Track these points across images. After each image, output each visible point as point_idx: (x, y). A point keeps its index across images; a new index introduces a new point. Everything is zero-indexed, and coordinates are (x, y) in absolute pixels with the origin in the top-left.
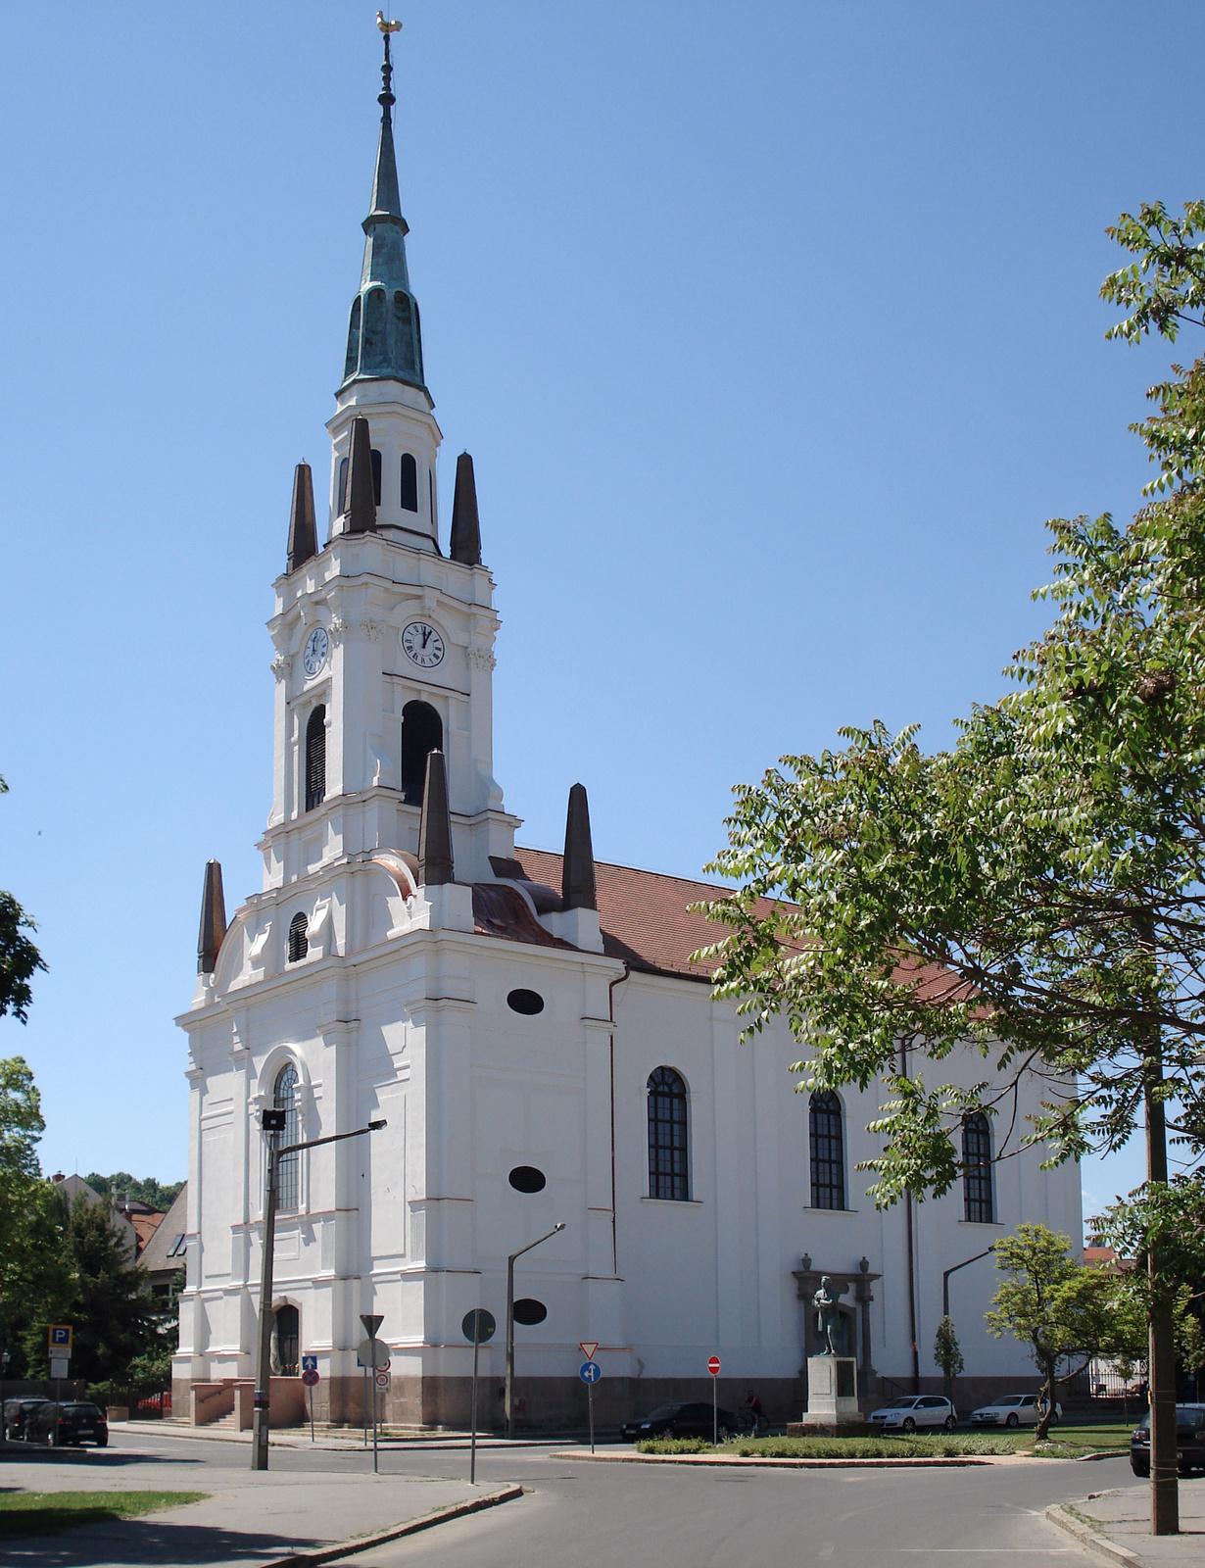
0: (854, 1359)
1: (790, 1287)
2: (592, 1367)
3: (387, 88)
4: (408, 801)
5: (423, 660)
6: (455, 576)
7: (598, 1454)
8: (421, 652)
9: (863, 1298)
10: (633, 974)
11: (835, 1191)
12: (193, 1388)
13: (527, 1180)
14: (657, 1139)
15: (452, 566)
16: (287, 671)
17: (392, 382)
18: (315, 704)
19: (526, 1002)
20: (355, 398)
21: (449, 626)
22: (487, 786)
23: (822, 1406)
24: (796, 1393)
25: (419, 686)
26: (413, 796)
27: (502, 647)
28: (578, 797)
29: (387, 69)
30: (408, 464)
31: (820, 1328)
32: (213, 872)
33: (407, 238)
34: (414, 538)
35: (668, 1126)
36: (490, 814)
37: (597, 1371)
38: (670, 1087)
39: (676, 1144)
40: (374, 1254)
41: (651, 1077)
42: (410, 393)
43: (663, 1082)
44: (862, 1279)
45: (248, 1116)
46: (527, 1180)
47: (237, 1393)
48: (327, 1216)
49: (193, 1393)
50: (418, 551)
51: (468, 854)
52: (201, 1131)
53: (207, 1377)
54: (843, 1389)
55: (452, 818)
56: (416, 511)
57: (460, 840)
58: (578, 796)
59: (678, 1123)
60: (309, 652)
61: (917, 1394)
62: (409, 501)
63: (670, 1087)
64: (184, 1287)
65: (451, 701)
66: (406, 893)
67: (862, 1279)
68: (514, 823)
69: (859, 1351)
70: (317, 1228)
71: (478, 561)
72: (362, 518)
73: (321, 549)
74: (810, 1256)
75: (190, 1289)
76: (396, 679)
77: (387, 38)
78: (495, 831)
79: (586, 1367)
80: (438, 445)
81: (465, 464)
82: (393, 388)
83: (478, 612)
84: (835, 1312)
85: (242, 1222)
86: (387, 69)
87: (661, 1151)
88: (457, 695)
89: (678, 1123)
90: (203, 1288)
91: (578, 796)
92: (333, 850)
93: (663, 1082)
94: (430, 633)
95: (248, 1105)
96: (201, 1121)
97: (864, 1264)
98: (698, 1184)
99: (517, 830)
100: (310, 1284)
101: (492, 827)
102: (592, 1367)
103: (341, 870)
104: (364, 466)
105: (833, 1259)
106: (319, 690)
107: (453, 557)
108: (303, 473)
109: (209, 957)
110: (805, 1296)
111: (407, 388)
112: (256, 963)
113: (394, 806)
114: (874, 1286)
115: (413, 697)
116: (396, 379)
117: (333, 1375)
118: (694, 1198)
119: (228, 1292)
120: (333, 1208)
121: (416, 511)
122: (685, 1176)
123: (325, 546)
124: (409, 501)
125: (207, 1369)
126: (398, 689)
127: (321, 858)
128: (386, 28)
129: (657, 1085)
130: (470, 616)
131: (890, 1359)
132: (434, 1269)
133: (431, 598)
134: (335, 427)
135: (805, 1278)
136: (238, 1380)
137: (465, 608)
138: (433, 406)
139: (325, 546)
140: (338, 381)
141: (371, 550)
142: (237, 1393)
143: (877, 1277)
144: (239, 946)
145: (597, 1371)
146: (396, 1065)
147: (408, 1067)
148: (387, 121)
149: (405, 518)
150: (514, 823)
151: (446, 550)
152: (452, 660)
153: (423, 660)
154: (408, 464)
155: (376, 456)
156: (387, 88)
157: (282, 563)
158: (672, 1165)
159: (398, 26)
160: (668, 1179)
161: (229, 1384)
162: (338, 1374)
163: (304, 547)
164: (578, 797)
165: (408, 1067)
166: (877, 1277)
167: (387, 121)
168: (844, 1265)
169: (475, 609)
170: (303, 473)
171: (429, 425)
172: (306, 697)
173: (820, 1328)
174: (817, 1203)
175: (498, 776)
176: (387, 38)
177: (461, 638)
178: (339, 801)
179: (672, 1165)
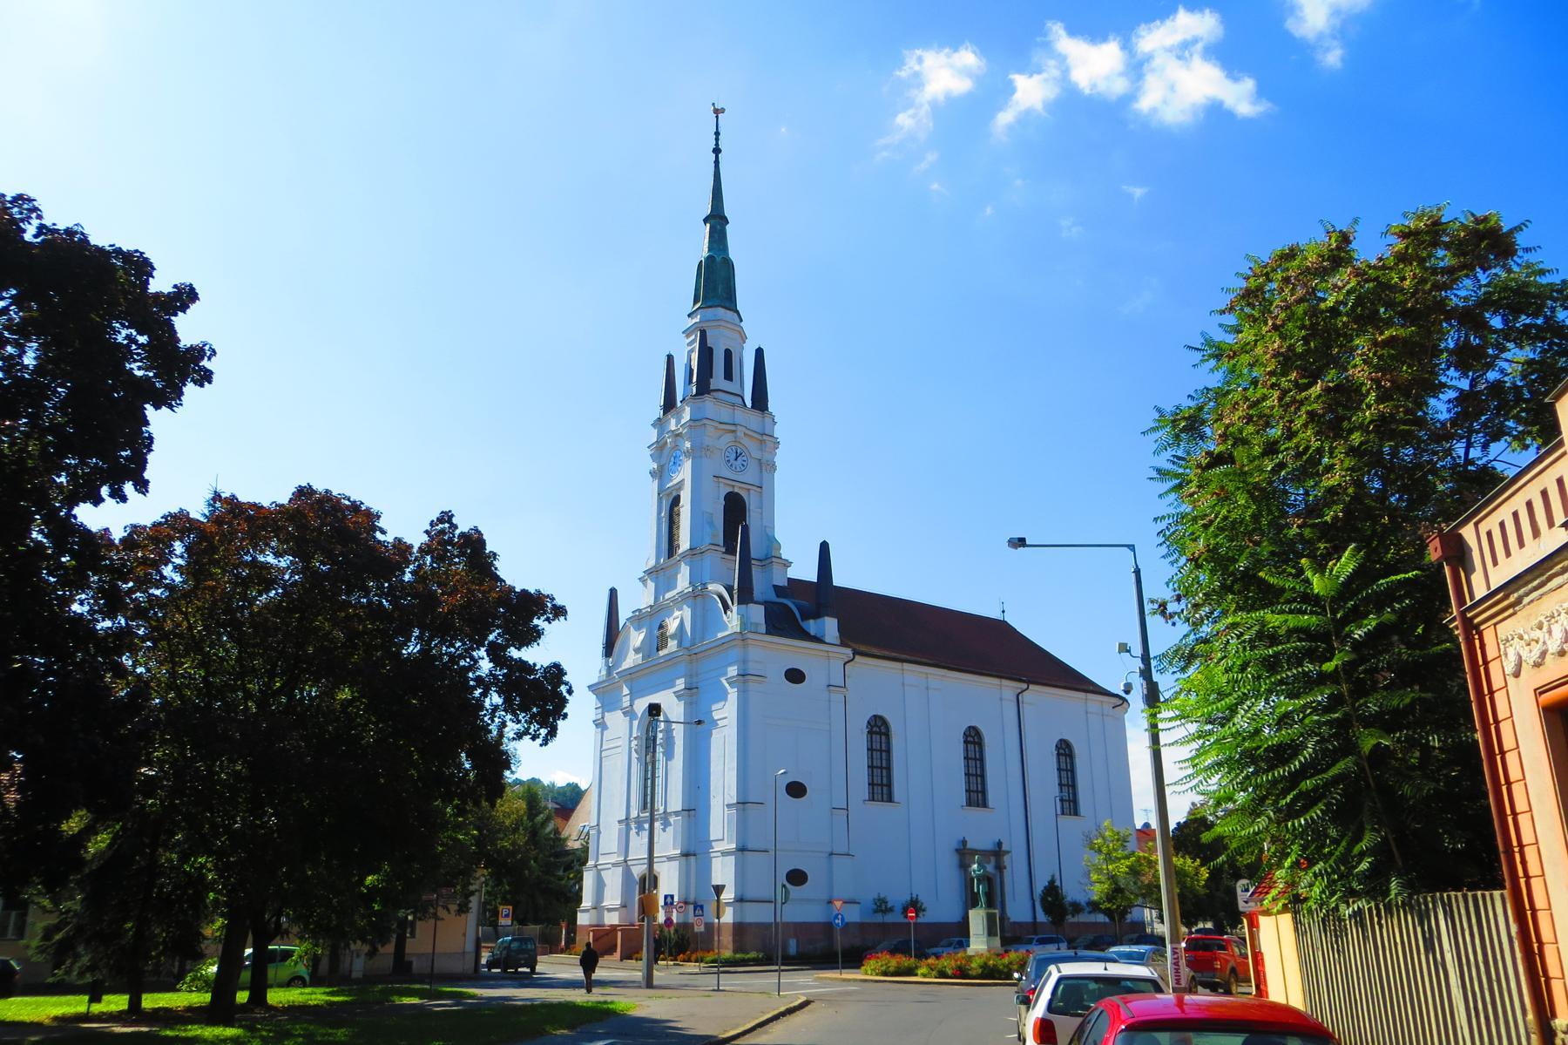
0: (997, 911)
1: (953, 860)
2: (840, 916)
3: (717, 144)
4: (727, 552)
5: (736, 468)
6: (753, 419)
7: (844, 976)
8: (732, 461)
9: (1000, 868)
10: (857, 657)
11: (884, 771)
12: (593, 931)
13: (796, 790)
14: (873, 779)
15: (813, 652)
16: (660, 474)
17: (720, 308)
18: (674, 494)
19: (795, 676)
20: (1125, 187)
21: (751, 446)
22: (772, 543)
23: (979, 944)
24: (961, 931)
25: (734, 483)
26: (730, 550)
27: (781, 458)
28: (824, 548)
29: (717, 134)
30: (728, 354)
31: (976, 890)
32: (613, 594)
33: (728, 227)
34: (732, 397)
35: (879, 770)
36: (772, 557)
37: (843, 919)
38: (879, 728)
39: (884, 765)
40: (711, 839)
41: (868, 722)
42: (729, 315)
43: (876, 725)
44: (997, 853)
45: (630, 748)
46: (796, 790)
47: (619, 934)
48: (676, 813)
49: (591, 934)
50: (733, 405)
51: (760, 587)
52: (601, 758)
53: (601, 923)
54: (991, 932)
55: (753, 562)
56: (732, 380)
57: (756, 572)
58: (824, 548)
59: (885, 768)
60: (672, 463)
61: (1037, 935)
62: (728, 375)
63: (879, 728)
64: (587, 862)
65: (751, 492)
66: (726, 607)
67: (997, 853)
68: (787, 564)
69: (998, 903)
70: (672, 819)
71: (767, 409)
72: (703, 388)
73: (679, 404)
74: (966, 839)
75: (591, 863)
76: (721, 480)
77: (717, 117)
78: (776, 568)
79: (836, 917)
80: (744, 342)
81: (759, 353)
82: (721, 311)
83: (767, 440)
84: (987, 880)
85: (624, 818)
86: (717, 134)
87: (875, 787)
88: (755, 488)
89: (885, 768)
90: (600, 862)
91: (824, 548)
92: (683, 582)
93: (876, 725)
94: (741, 454)
95: (630, 742)
96: (601, 752)
97: (1000, 844)
98: (991, 803)
99: (789, 569)
100: (665, 859)
101: (775, 566)
102: (840, 916)
103: (689, 595)
104: (706, 354)
105: (980, 841)
106: (678, 486)
107: (752, 407)
108: (670, 359)
109: (609, 648)
110: (964, 866)
111: (728, 311)
112: (637, 651)
113: (720, 555)
114: (1006, 859)
115: (731, 490)
116: (723, 307)
117: (736, 921)
118: (896, 800)
119: (614, 865)
120: (680, 809)
121: (732, 380)
122: (889, 785)
123: (681, 402)
124: (728, 375)
125: (601, 917)
126: (721, 485)
127: (676, 588)
128: (717, 112)
129: (872, 727)
130: (762, 442)
131: (1019, 909)
132: (742, 849)
133: (740, 432)
134: (687, 333)
135: (964, 853)
136: (621, 926)
137: (759, 437)
138: (741, 320)
139: (681, 402)
140: (689, 307)
141: (709, 405)
142: (619, 934)
143: (1008, 852)
144: (627, 638)
145: (843, 919)
146: (713, 709)
147: (725, 718)
148: (717, 162)
149: (725, 385)
150: (787, 564)
151: (749, 403)
152: (752, 468)
153: (736, 468)
154: (728, 354)
155: (711, 350)
156: (717, 144)
157: (659, 413)
158: (882, 779)
159: (723, 111)
160: (880, 788)
161: (614, 928)
162: (738, 920)
163: (669, 404)
164: (824, 548)
165: (725, 718)
166: (1008, 852)
167: (717, 162)
168: (986, 844)
169: (765, 437)
170: (670, 359)
171: (739, 332)
172: (670, 490)
173: (976, 890)
174: (969, 804)
175: (779, 535)
176: (717, 117)
177: (756, 454)
178: (687, 553)
179: (882, 779)
